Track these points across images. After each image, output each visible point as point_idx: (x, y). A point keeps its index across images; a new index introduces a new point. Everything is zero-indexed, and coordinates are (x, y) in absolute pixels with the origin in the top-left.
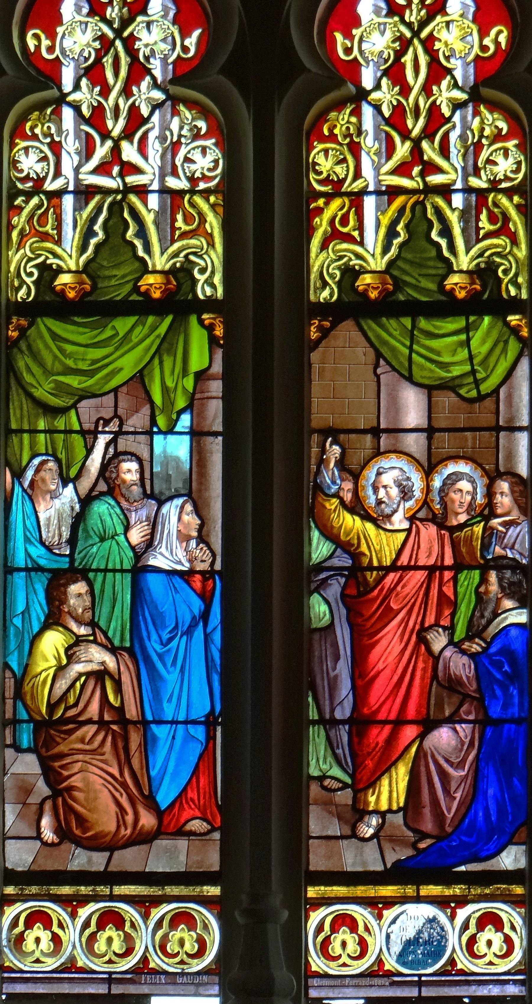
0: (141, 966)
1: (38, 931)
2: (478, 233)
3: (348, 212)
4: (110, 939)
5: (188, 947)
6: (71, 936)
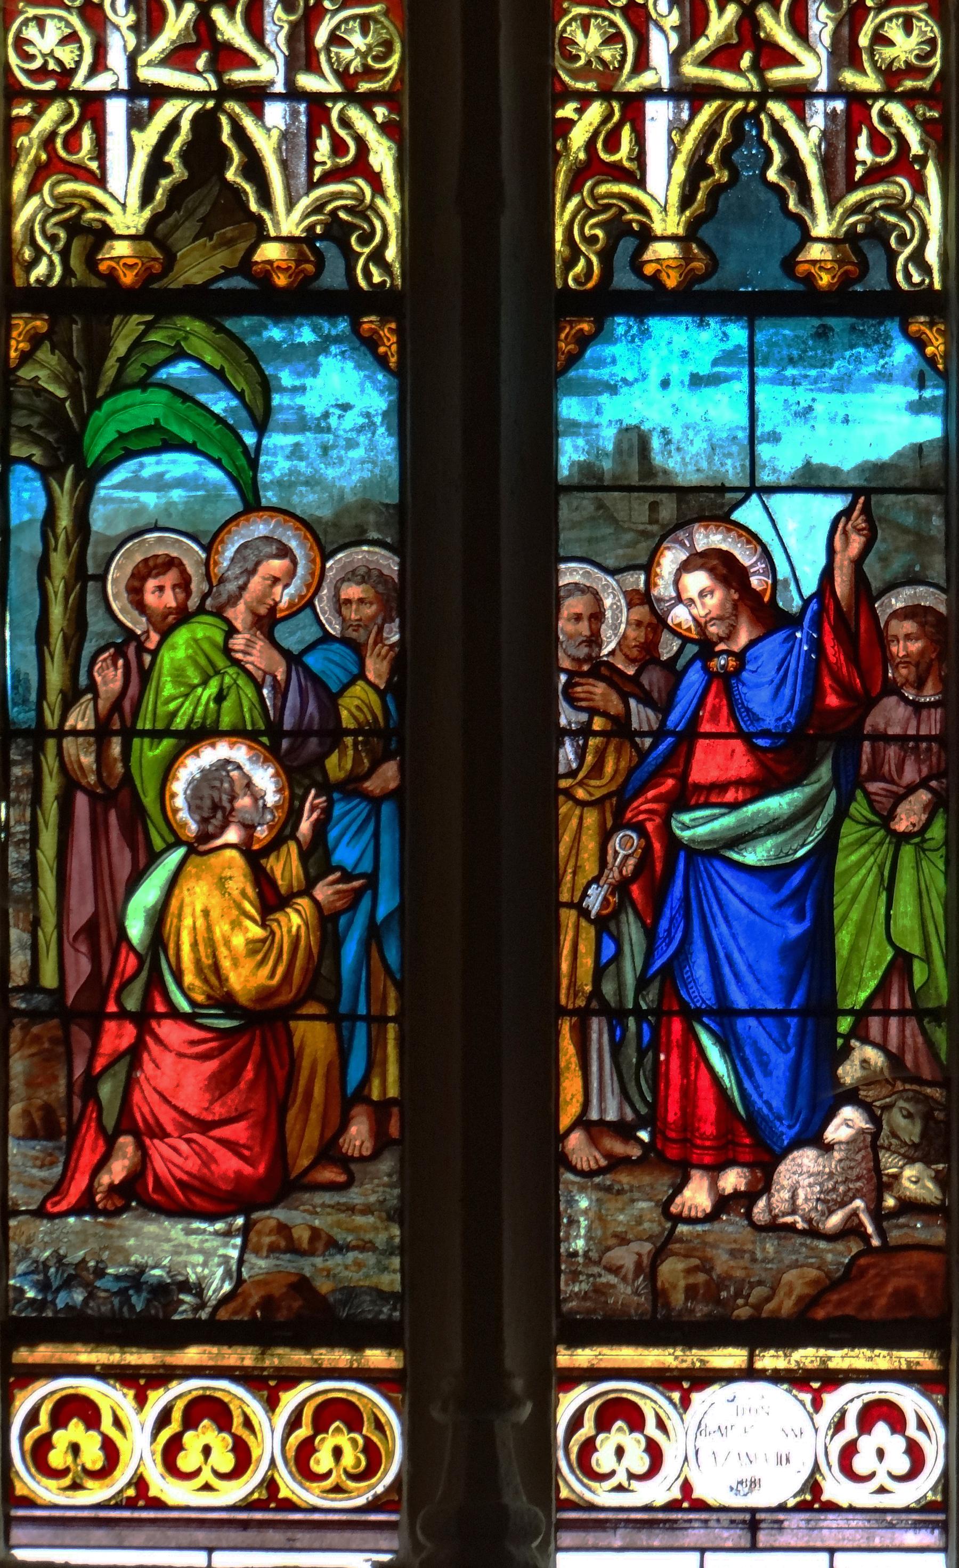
0: (808, 1497)
1: (619, 1434)
2: (851, 171)
3: (77, 129)
4: (206, 1444)
5: (348, 1459)
6: (269, 1440)
